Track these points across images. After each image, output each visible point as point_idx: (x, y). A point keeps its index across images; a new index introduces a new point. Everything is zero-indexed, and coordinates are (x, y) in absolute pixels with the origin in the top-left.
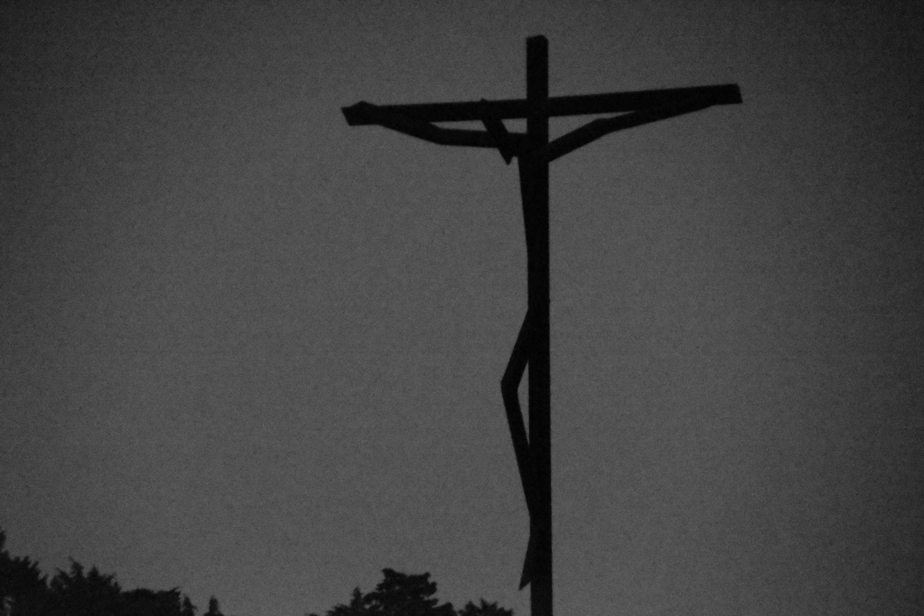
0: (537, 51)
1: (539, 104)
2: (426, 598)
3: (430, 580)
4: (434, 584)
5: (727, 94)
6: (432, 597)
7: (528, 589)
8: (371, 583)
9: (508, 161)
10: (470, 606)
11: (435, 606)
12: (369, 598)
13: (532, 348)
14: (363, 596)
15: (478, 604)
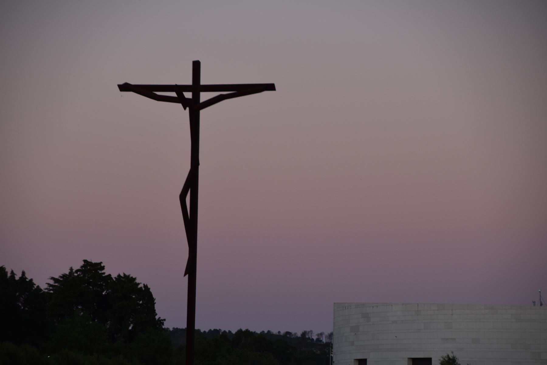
0: (196, 65)
1: (197, 87)
2: (100, 272)
3: (102, 265)
4: (104, 266)
5: (271, 87)
6: (103, 272)
7: (187, 276)
8: (77, 265)
9: (185, 109)
10: (119, 276)
12: (77, 271)
13: (192, 183)
15: (122, 275)
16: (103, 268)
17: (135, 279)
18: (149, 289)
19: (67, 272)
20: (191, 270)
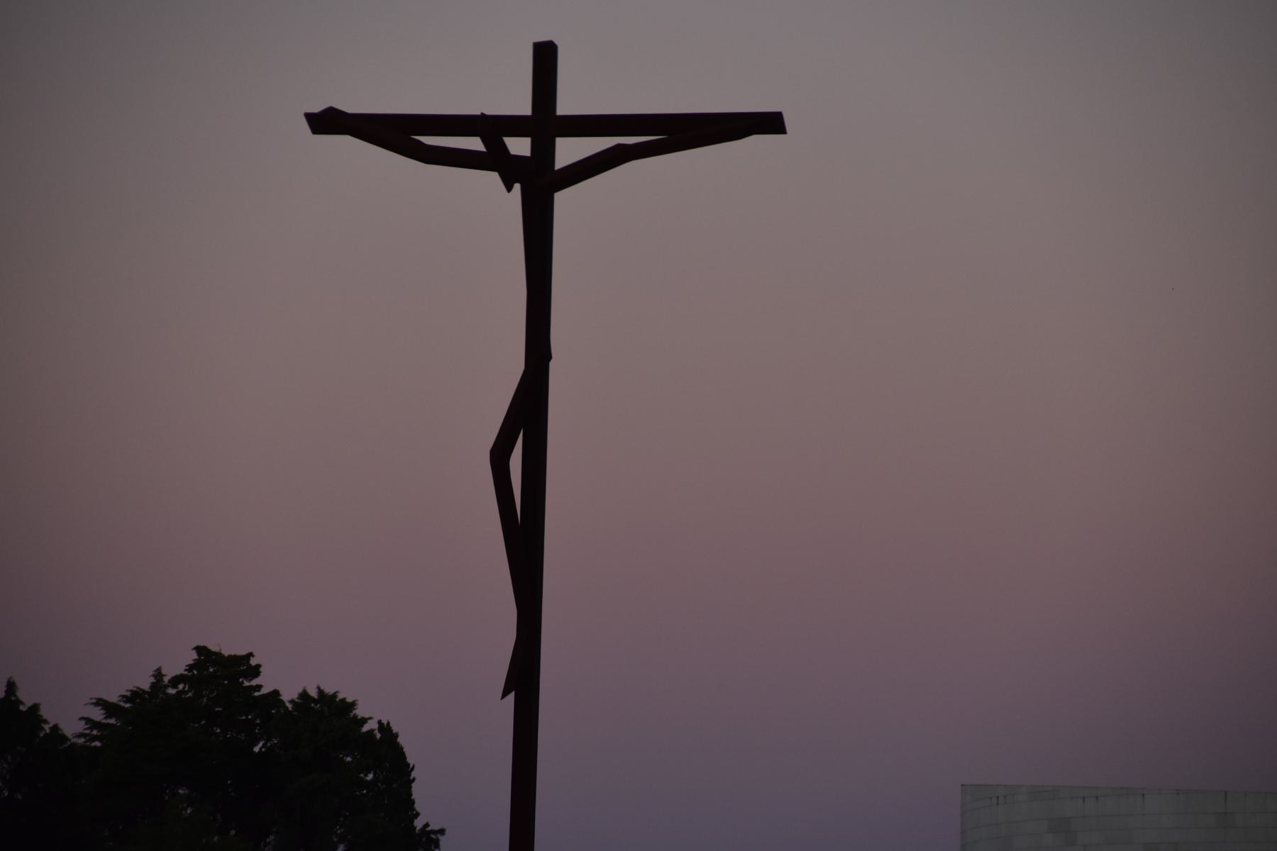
0: (545, 58)
1: (545, 122)
2: (246, 684)
3: (253, 662)
5: (771, 123)
6: (254, 682)
7: (511, 697)
8: (178, 662)
9: (509, 189)
10: (304, 695)
11: (257, 694)
12: (175, 681)
13: (528, 413)
14: (166, 680)
15: (313, 693)
16: (256, 671)
17: (352, 705)
18: (396, 736)
19: (145, 684)
20: (523, 677)
